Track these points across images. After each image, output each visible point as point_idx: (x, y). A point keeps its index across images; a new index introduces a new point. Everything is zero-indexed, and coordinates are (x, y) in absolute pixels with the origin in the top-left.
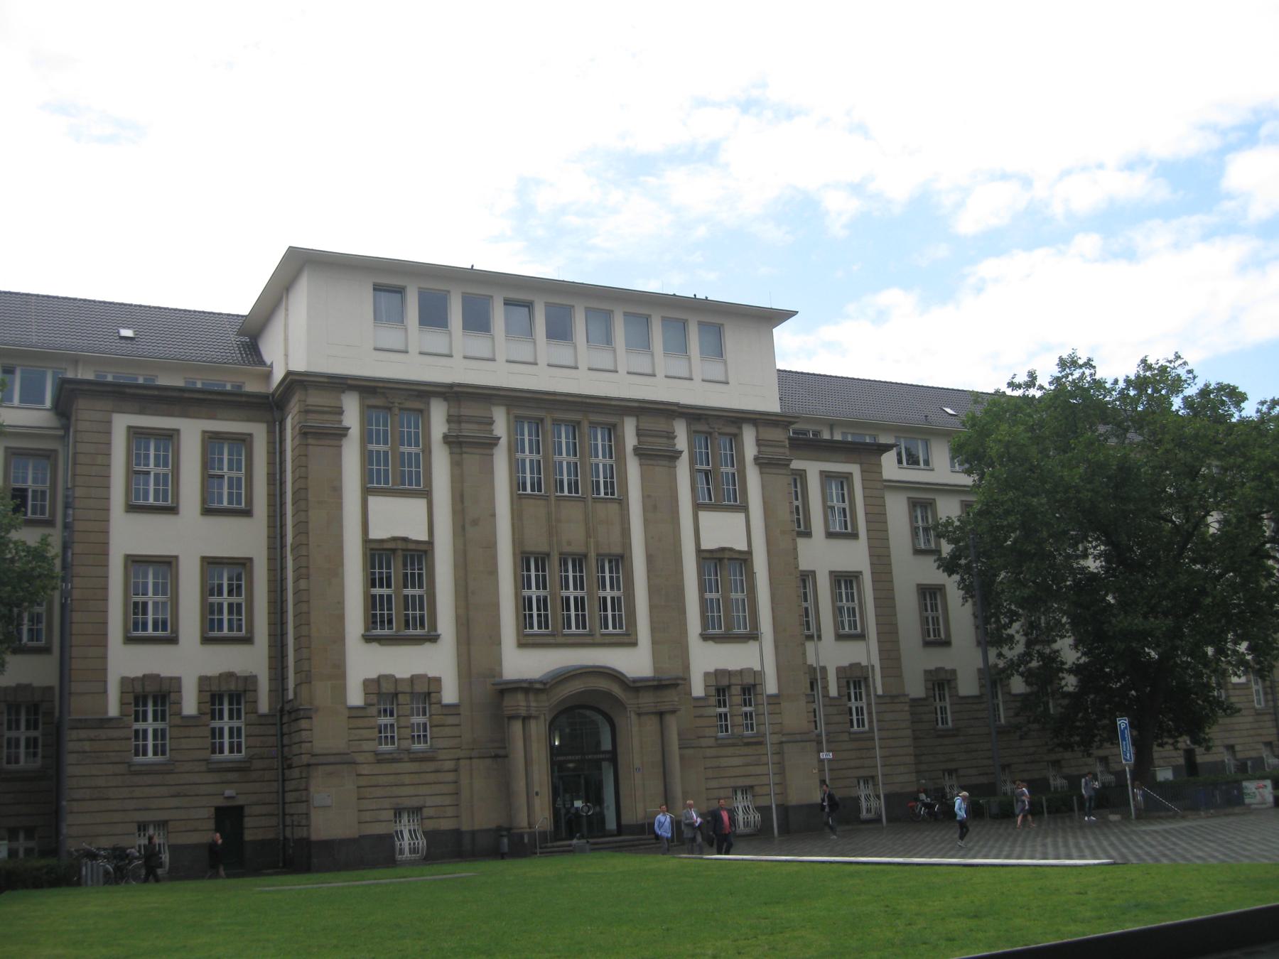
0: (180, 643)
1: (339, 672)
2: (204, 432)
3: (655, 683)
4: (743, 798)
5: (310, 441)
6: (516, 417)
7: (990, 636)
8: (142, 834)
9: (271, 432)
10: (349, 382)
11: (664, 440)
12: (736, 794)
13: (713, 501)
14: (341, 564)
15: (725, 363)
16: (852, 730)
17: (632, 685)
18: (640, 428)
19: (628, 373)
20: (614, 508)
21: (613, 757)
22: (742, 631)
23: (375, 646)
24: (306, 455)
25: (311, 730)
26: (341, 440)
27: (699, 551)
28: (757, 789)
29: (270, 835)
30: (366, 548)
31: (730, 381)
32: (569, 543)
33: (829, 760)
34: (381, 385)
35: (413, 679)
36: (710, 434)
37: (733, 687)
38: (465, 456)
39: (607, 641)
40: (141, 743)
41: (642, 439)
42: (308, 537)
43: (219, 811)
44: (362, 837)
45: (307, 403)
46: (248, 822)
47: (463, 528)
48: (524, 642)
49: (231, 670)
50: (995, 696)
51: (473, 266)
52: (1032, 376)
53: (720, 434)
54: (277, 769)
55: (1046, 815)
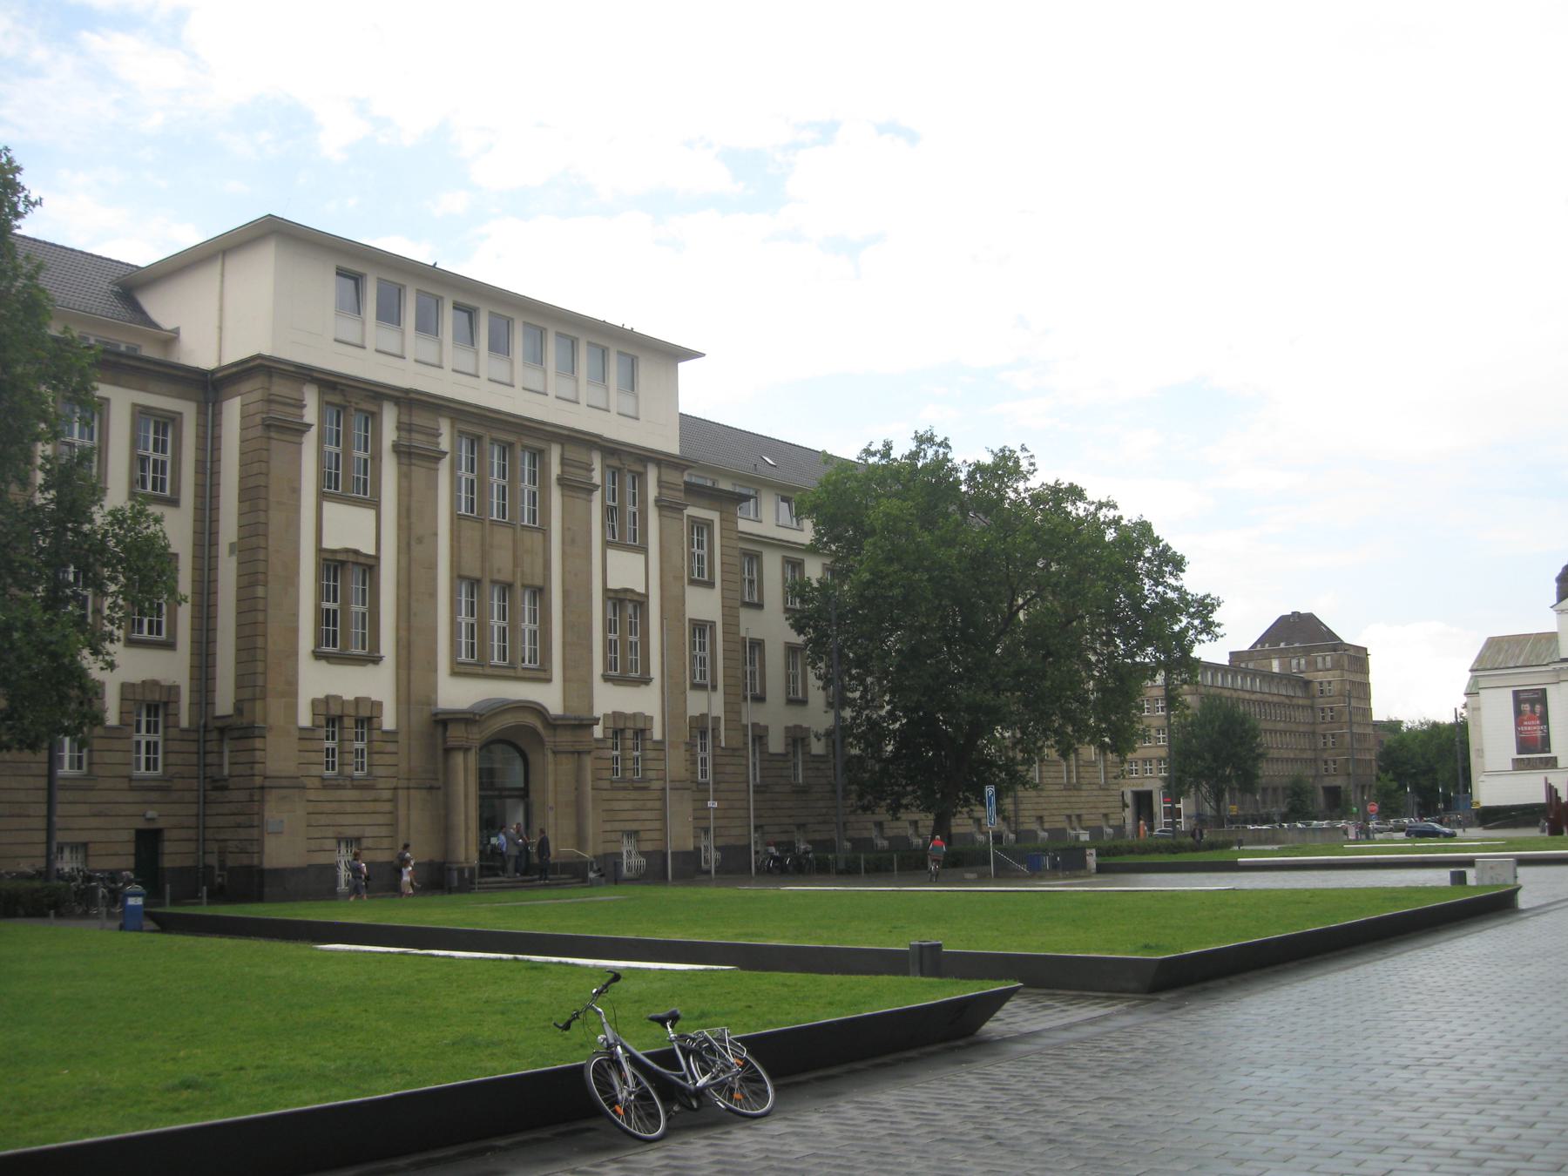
0: (178, 651)
1: (291, 690)
2: (134, 405)
3: (577, 722)
4: (347, 851)
5: (273, 435)
6: (459, 431)
7: (837, 702)
8: (74, 858)
9: (202, 413)
10: (315, 374)
11: (583, 472)
12: (339, 846)
13: (617, 539)
14: (297, 573)
15: (637, 397)
16: (136, 773)
17: (551, 721)
18: (401, 420)
19: (336, 340)
20: (538, 537)
21: (524, 794)
22: (359, 651)
23: (323, 663)
24: (267, 450)
25: (264, 750)
26: (302, 436)
27: (606, 590)
28: (642, 834)
29: (189, 862)
30: (320, 558)
31: (641, 417)
32: (499, 571)
33: (715, 809)
34: (344, 381)
35: (358, 700)
36: (344, 408)
37: (627, 731)
38: (413, 467)
39: (527, 676)
40: (360, 760)
41: (567, 468)
42: (267, 540)
43: (140, 834)
44: (310, 866)
45: (272, 392)
46: (168, 847)
47: (409, 545)
48: (458, 671)
49: (156, 678)
50: (795, 754)
51: (435, 264)
52: (888, 447)
53: (356, 410)
54: (198, 790)
55: (896, 872)
